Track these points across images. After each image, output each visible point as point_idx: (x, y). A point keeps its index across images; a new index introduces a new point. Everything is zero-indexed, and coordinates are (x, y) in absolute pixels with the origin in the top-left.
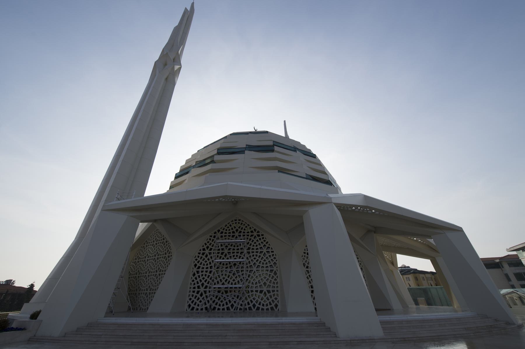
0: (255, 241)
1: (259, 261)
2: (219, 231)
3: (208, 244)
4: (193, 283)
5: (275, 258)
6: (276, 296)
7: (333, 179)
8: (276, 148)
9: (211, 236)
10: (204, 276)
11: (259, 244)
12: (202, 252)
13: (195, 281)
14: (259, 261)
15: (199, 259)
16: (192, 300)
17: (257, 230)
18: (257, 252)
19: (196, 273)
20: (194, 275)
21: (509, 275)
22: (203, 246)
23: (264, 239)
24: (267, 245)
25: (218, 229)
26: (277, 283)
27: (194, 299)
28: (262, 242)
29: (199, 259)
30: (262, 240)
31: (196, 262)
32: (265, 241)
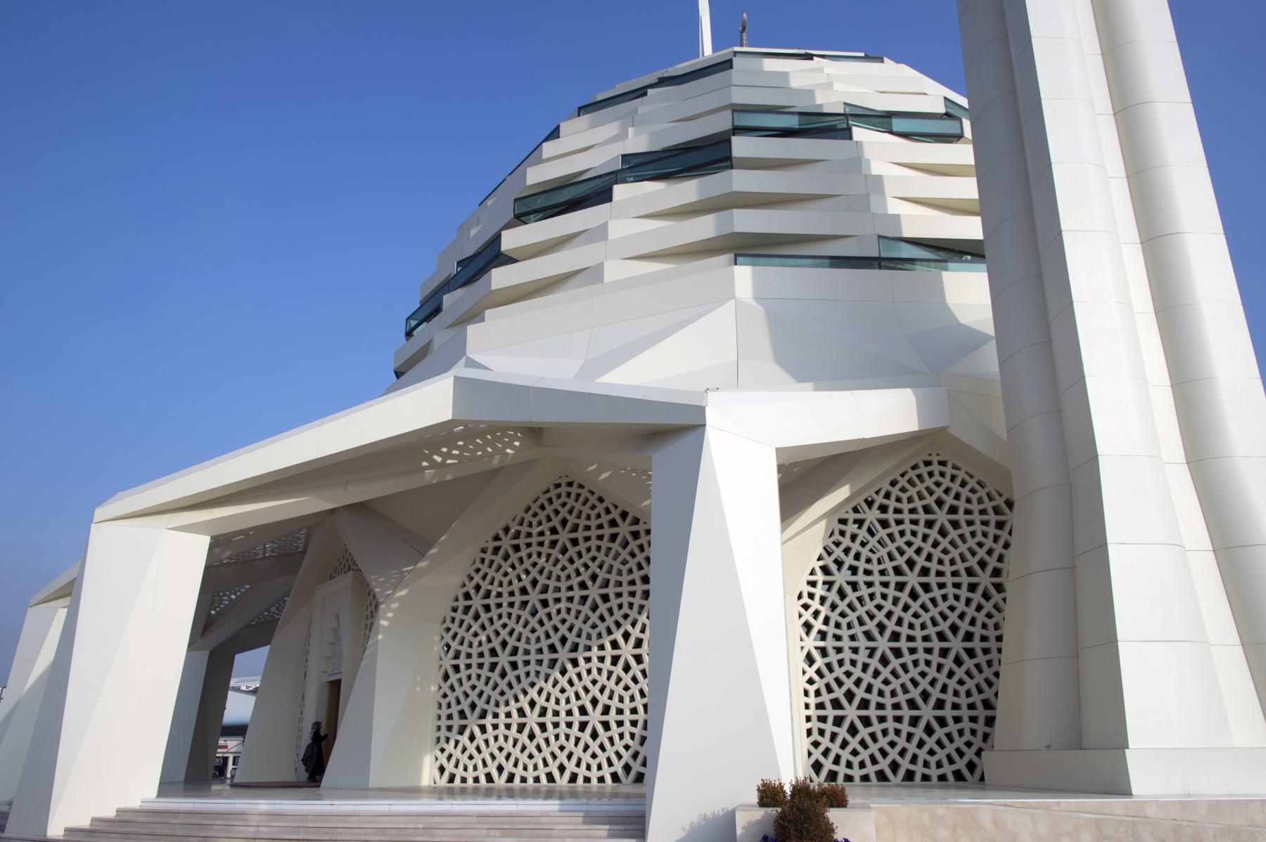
0: (858, 630)
2: (639, 659)
4: (444, 702)
5: (811, 681)
8: (741, 146)
9: (843, 521)
12: (462, 603)
13: (451, 698)
15: (455, 628)
18: (921, 744)
19: (451, 672)
20: (446, 677)
23: (837, 537)
25: (646, 658)
26: (809, 732)
31: (448, 637)
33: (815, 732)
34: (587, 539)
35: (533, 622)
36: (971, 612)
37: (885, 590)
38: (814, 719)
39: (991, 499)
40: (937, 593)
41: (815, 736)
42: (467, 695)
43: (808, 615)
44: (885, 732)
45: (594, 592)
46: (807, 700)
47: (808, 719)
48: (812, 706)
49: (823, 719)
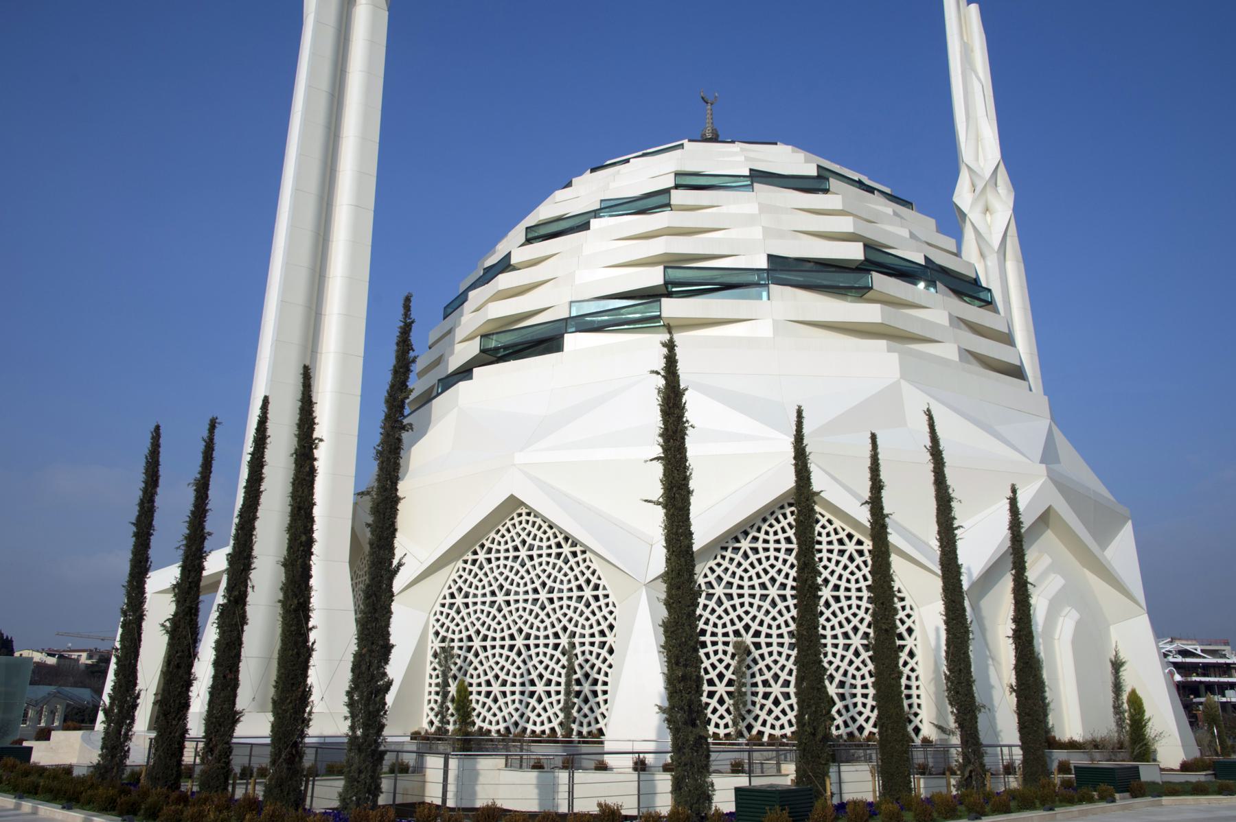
3: (602, 602)
5: (909, 616)
6: (611, 608)
10: (544, 566)
11: (727, 569)
12: (594, 580)
13: (605, 611)
22: (604, 588)
26: (917, 679)
27: (850, 714)
28: (734, 573)
33: (913, 679)
34: (540, 556)
35: (587, 612)
36: (839, 570)
37: (780, 649)
38: (914, 687)
39: (836, 533)
40: (756, 582)
41: (913, 675)
42: (583, 574)
44: (850, 607)
48: (915, 697)
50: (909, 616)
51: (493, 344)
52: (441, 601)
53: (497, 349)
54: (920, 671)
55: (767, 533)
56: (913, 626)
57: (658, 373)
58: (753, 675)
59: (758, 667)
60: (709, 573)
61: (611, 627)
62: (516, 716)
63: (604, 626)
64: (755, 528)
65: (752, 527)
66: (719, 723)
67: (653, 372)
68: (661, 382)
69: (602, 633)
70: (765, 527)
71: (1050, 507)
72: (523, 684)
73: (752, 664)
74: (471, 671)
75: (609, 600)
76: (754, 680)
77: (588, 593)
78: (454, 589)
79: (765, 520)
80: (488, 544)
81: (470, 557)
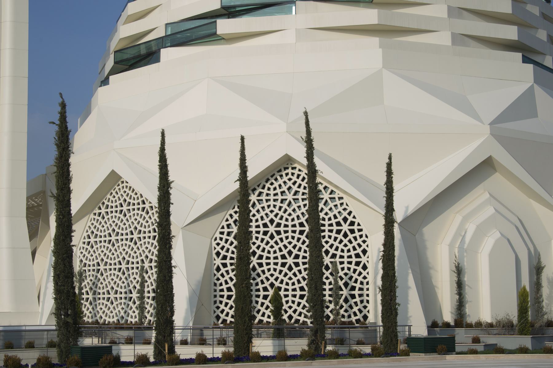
1: (297, 185)
3: (357, 234)
6: (364, 238)
7: (489, 177)
12: (350, 219)
13: (360, 241)
14: (297, 185)
16: (220, 246)
17: (331, 188)
21: (467, 233)
22: (359, 225)
23: (344, 206)
24: (350, 219)
26: (368, 283)
29: (222, 243)
30: (340, 209)
32: (345, 209)
33: (365, 284)
38: (365, 290)
41: (365, 281)
43: (364, 273)
45: (272, 229)
46: (368, 298)
47: (368, 289)
48: (365, 295)
49: (361, 289)
50: (364, 242)
51: (126, 56)
52: (83, 240)
53: (128, 60)
54: (370, 278)
55: (269, 189)
56: (366, 248)
57: (54, 123)
58: (257, 284)
59: (261, 278)
60: (229, 218)
61: (364, 252)
62: (122, 313)
63: (359, 251)
64: (261, 186)
65: (258, 186)
66: (264, 313)
67: (50, 123)
68: (56, 128)
69: (358, 256)
70: (268, 185)
71: (491, 156)
72: (126, 293)
73: (256, 277)
74: (99, 285)
75: (363, 233)
76: (258, 287)
77: (345, 227)
78: (89, 233)
79: (267, 181)
80: (106, 203)
81: (97, 211)
